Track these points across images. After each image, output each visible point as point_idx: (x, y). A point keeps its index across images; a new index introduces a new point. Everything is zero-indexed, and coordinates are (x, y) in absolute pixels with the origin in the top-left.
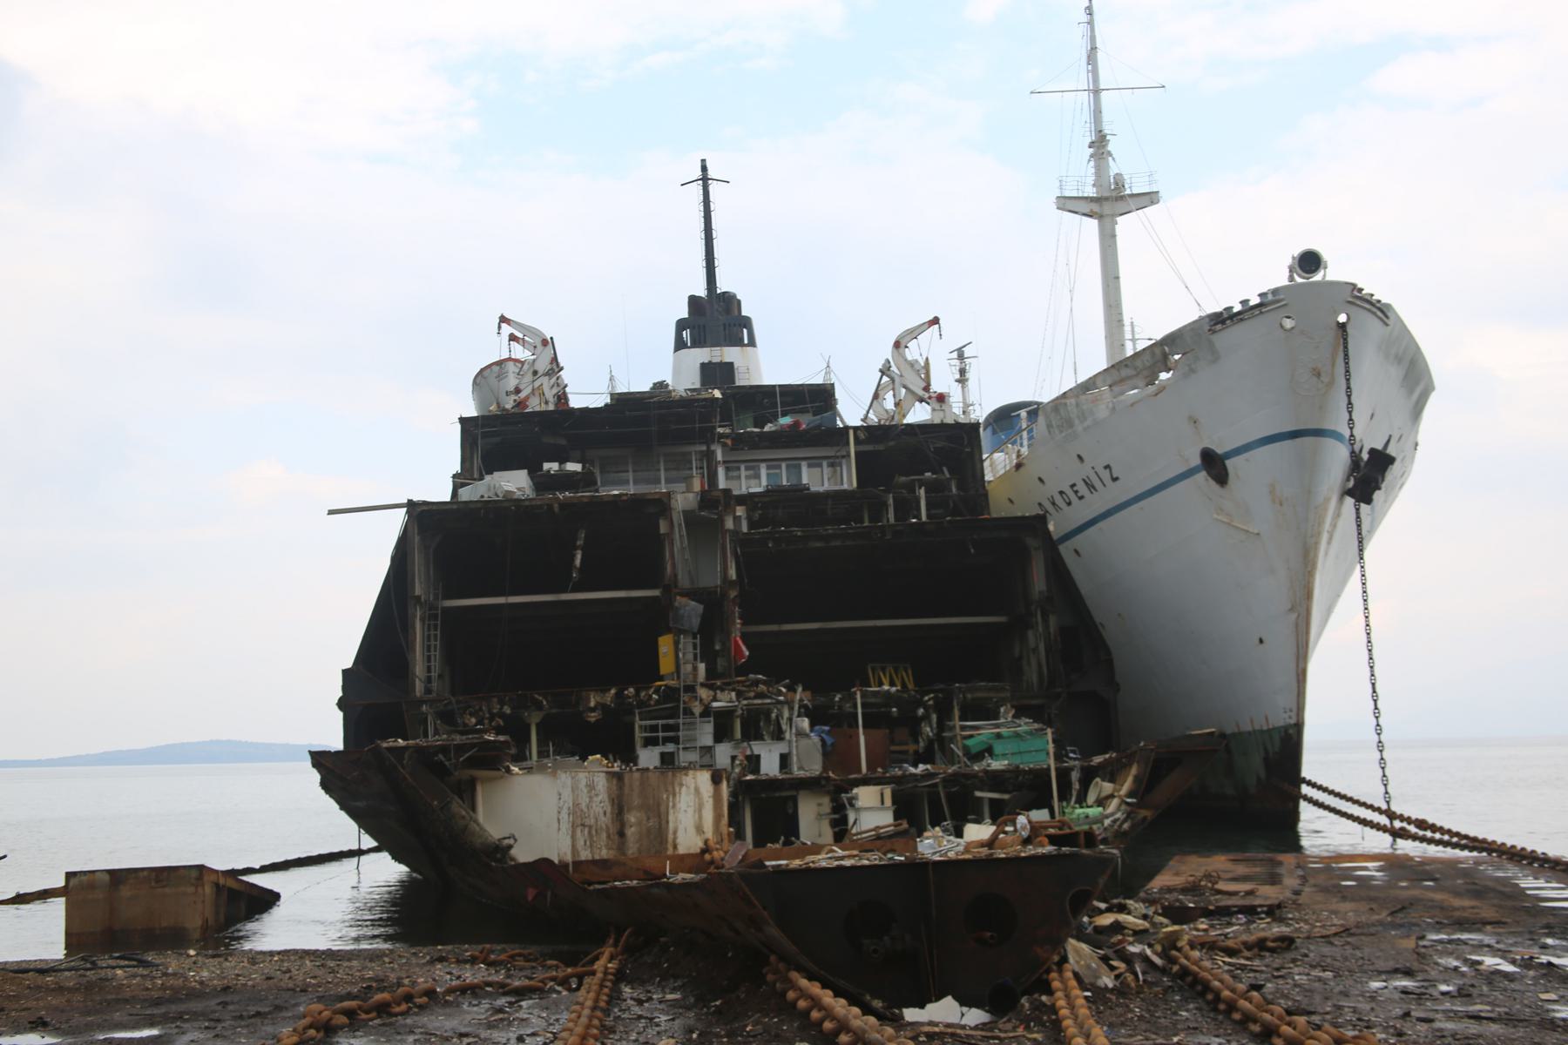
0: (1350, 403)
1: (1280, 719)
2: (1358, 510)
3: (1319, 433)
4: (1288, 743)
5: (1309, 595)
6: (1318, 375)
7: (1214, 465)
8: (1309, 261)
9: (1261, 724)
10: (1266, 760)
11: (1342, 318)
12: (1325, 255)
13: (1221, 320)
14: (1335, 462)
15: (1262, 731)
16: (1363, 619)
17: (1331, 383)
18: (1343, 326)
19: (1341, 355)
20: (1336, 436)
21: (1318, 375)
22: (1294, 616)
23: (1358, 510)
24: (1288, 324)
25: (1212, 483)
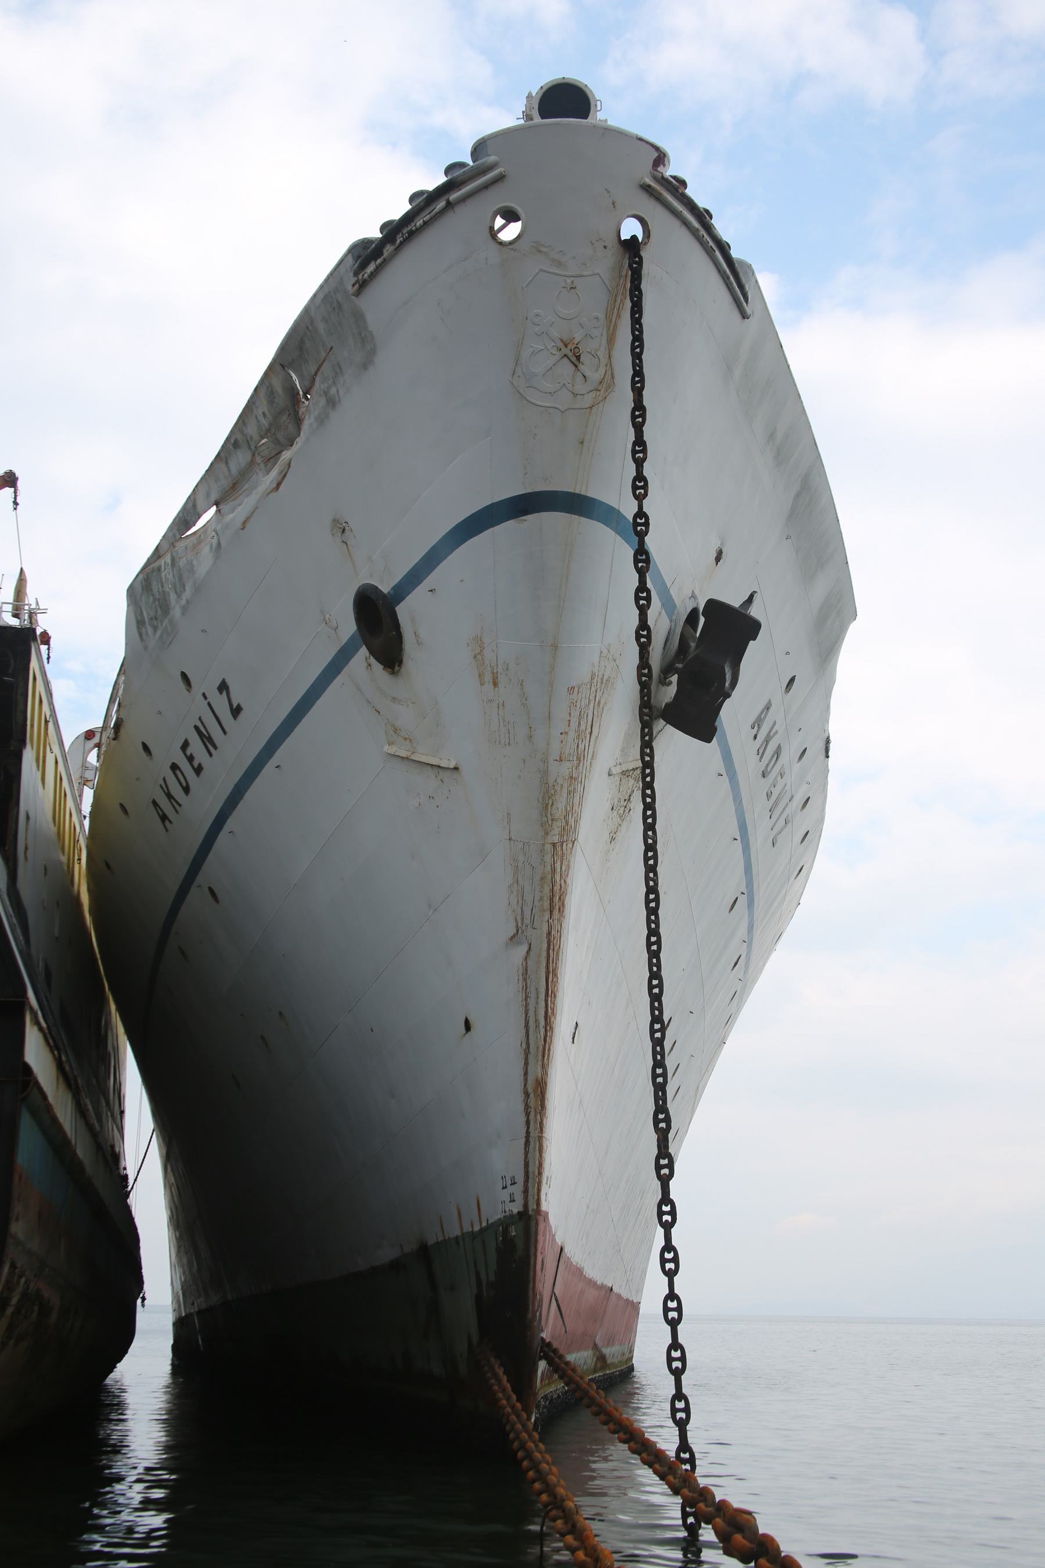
0: (640, 443)
1: (499, 1204)
2: (647, 745)
3: (577, 504)
4: (517, 1239)
5: (554, 903)
6: (575, 359)
7: (378, 623)
8: (565, 100)
9: (473, 1223)
10: (478, 1299)
11: (631, 228)
12: (597, 90)
13: (367, 259)
14: (606, 644)
15: (473, 1235)
16: (653, 1137)
17: (607, 384)
18: (632, 246)
19: (624, 336)
20: (608, 515)
21: (575, 359)
22: (521, 951)
23: (647, 745)
24: (511, 232)
25: (377, 667)
